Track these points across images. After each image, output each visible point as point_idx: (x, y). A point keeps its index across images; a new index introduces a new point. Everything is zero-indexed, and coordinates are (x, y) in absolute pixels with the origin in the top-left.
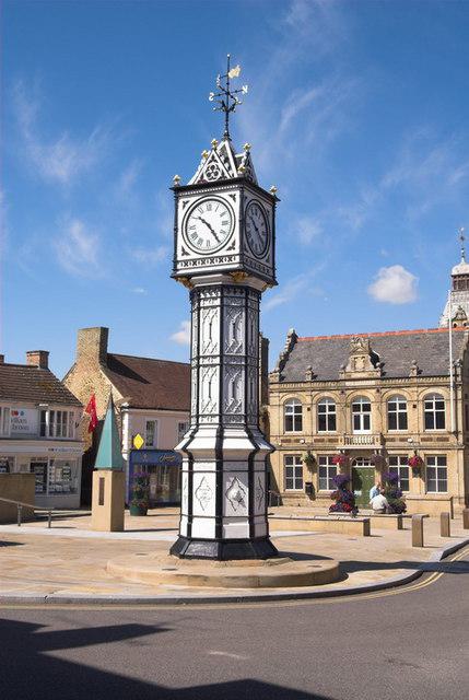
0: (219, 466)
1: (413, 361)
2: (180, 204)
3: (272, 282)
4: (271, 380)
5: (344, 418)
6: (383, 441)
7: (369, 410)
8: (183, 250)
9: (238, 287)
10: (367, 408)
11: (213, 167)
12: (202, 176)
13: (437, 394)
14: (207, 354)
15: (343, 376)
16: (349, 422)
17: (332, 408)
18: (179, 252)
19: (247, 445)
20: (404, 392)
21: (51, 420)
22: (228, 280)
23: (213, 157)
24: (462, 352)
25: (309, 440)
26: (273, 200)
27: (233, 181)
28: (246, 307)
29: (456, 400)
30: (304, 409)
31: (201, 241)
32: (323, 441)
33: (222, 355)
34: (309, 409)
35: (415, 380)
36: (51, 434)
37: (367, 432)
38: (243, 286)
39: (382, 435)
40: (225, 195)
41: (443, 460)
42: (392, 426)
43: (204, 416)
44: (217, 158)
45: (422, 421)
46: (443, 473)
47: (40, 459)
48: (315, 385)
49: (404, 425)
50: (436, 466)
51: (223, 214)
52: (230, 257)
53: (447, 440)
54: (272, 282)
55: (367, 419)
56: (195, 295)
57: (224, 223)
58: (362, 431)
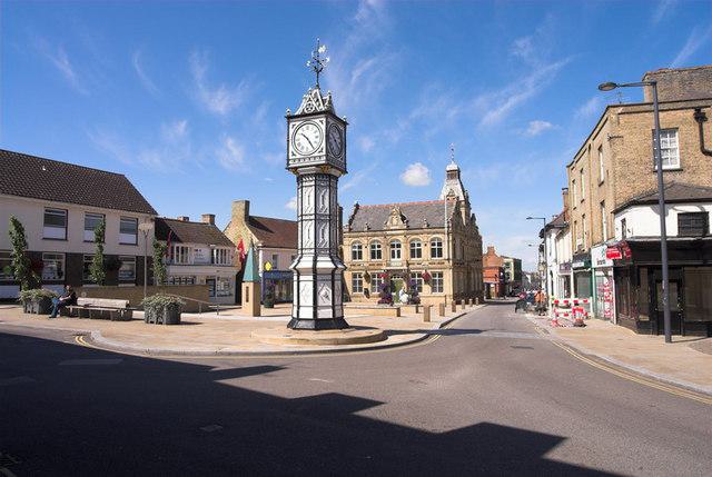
0: (315, 278)
3: (345, 172)
5: (386, 252)
6: (408, 264)
10: (399, 246)
17: (379, 246)
26: (345, 124)
33: (315, 214)
40: (317, 121)
41: (441, 275)
42: (413, 256)
46: (441, 282)
49: (419, 256)
54: (345, 172)
55: (399, 252)
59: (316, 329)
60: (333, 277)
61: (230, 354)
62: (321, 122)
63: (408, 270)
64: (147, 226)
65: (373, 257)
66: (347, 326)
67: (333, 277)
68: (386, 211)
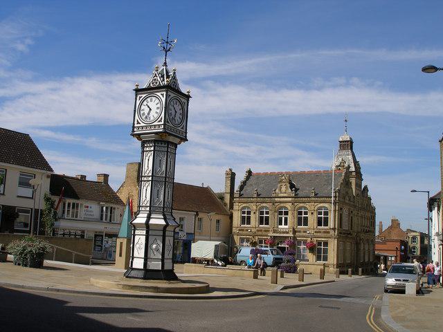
0: (147, 232)
2: (138, 98)
3: (185, 139)
4: (235, 196)
5: (273, 219)
6: (294, 232)
7: (287, 214)
10: (286, 213)
13: (325, 207)
14: (146, 175)
15: (274, 195)
16: (276, 221)
17: (267, 213)
18: (136, 122)
19: (163, 222)
20: (307, 205)
22: (157, 137)
24: (339, 184)
25: (253, 230)
26: (188, 97)
27: (164, 87)
28: (167, 152)
29: (335, 211)
30: (252, 213)
32: (261, 231)
33: (152, 176)
34: (254, 213)
38: (168, 139)
40: (158, 94)
41: (326, 244)
43: (142, 207)
45: (316, 221)
46: (326, 251)
47: (100, 232)
49: (306, 224)
52: (159, 125)
53: (328, 232)
54: (185, 139)
55: (286, 219)
56: (143, 143)
57: (158, 108)
58: (283, 226)
59: (145, 278)
60: (164, 233)
61: (58, 290)
62: (162, 95)
63: (295, 238)
65: (261, 223)
66: (175, 278)
67: (164, 233)
68: (275, 178)
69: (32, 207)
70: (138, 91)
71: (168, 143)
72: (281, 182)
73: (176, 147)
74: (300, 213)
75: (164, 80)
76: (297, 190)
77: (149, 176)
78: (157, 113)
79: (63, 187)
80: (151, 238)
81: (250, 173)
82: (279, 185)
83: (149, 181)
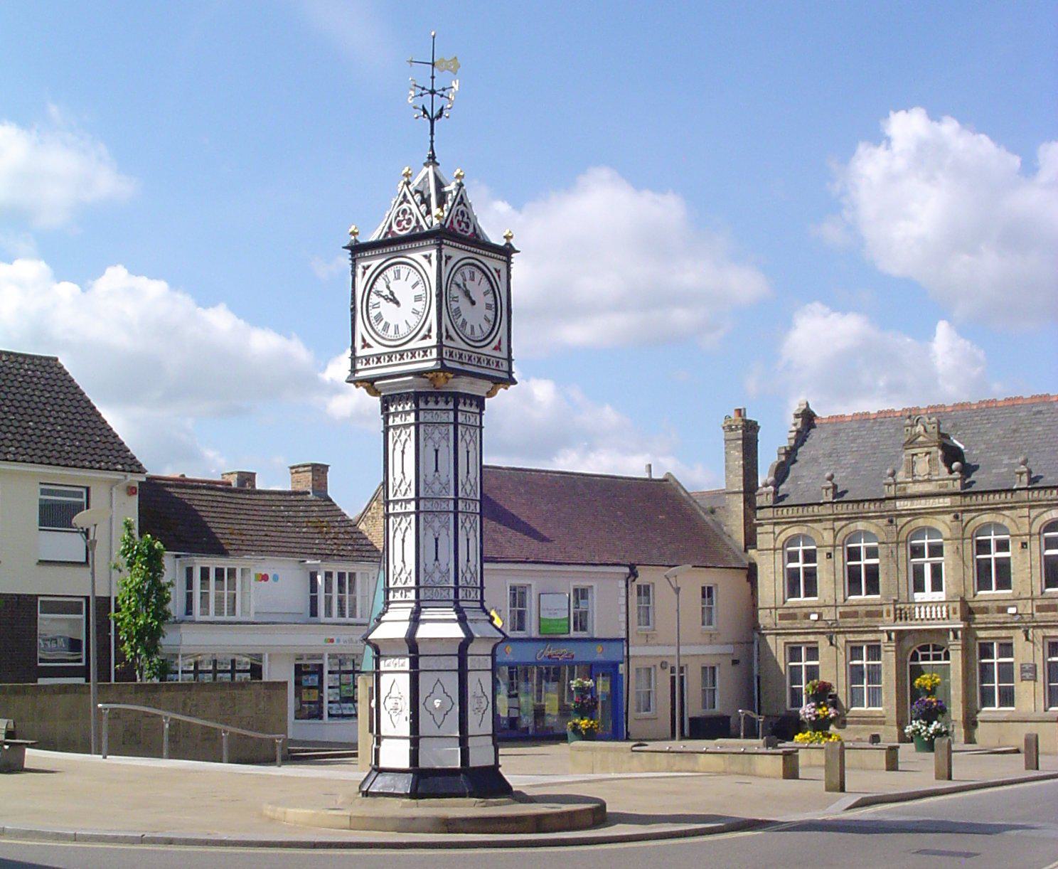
0: (414, 663)
1: (1021, 459)
2: (360, 271)
4: (760, 501)
6: (968, 613)
8: (364, 340)
9: (442, 394)
10: (936, 550)
11: (404, 212)
12: (390, 227)
14: (399, 497)
15: (892, 492)
18: (359, 343)
19: (456, 631)
20: (1005, 519)
21: (328, 588)
22: (423, 385)
23: (405, 196)
25: (829, 615)
26: (506, 252)
30: (821, 556)
31: (387, 326)
33: (417, 499)
34: (829, 556)
35: (1024, 494)
36: (329, 613)
37: (940, 596)
38: (449, 389)
39: (963, 602)
40: (418, 256)
42: (984, 583)
43: (396, 590)
44: (409, 197)
48: (841, 509)
49: (1004, 583)
50: (865, 662)
51: (417, 284)
52: (425, 350)
55: (936, 570)
57: (418, 298)
62: (425, 260)
64: (113, 512)
68: (899, 429)
69: (89, 593)
70: (358, 250)
71: (457, 397)
72: (911, 443)
73: (481, 405)
74: (983, 547)
75: (429, 212)
76: (967, 470)
77: (408, 501)
78: (415, 312)
79: (179, 518)
80: (425, 681)
81: (808, 418)
82: (905, 456)
83: (408, 514)
